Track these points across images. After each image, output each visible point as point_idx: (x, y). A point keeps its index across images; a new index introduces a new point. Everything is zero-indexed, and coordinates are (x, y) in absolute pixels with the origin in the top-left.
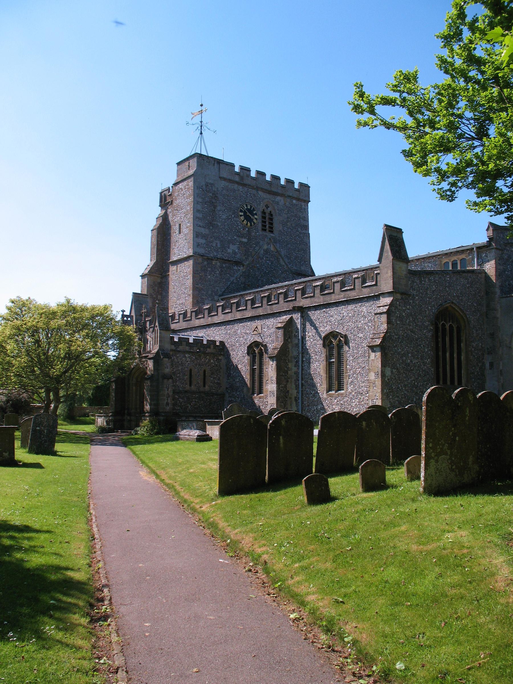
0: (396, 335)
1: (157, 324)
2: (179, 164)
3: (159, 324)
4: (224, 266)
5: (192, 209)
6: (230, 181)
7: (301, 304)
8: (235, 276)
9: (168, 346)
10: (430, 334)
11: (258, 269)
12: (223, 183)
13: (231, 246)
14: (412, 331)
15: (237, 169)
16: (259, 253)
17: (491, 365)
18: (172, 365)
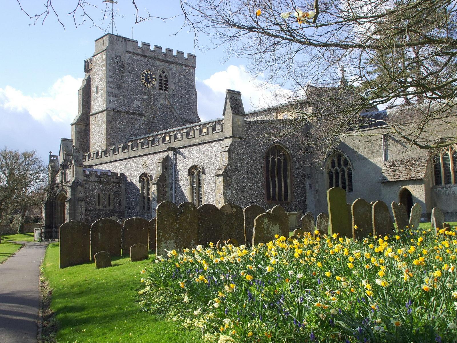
0: (235, 167)
1: (73, 162)
2: (96, 41)
3: (75, 162)
4: (130, 117)
5: (105, 75)
6: (134, 53)
7: (174, 146)
8: (139, 124)
9: (81, 178)
10: (262, 165)
11: (157, 119)
12: (129, 55)
13: (136, 102)
14: (248, 164)
15: (140, 45)
16: (157, 107)
17: (310, 186)
18: (85, 191)
